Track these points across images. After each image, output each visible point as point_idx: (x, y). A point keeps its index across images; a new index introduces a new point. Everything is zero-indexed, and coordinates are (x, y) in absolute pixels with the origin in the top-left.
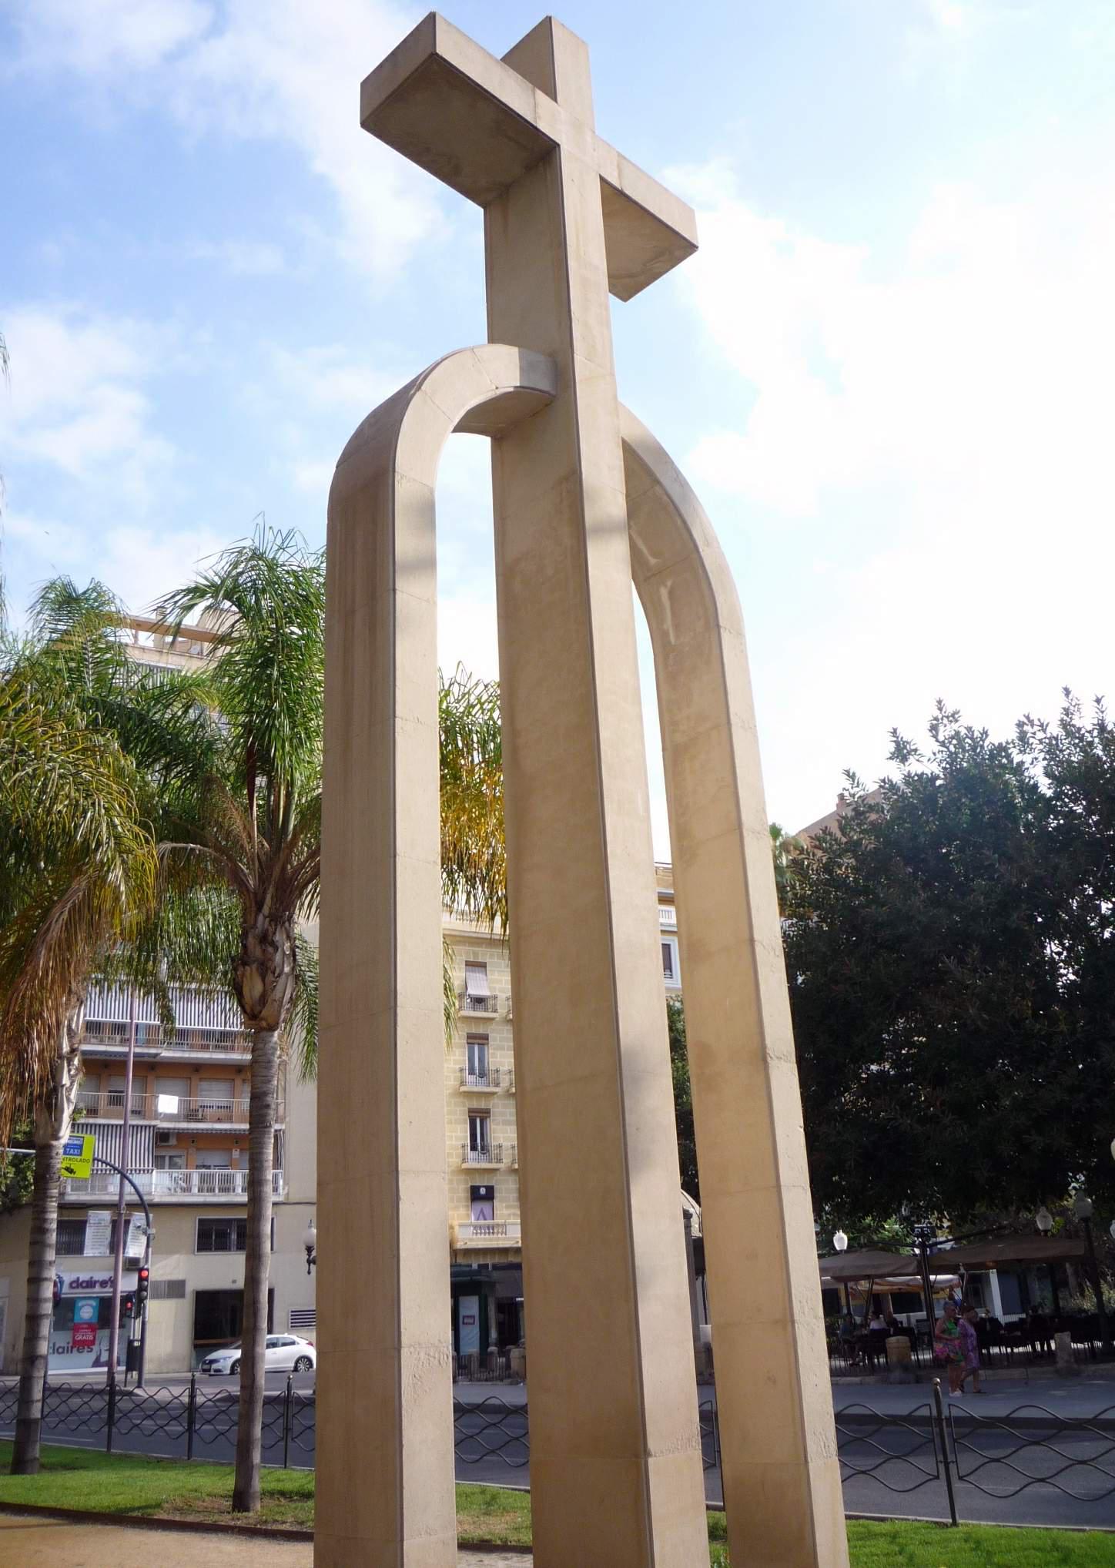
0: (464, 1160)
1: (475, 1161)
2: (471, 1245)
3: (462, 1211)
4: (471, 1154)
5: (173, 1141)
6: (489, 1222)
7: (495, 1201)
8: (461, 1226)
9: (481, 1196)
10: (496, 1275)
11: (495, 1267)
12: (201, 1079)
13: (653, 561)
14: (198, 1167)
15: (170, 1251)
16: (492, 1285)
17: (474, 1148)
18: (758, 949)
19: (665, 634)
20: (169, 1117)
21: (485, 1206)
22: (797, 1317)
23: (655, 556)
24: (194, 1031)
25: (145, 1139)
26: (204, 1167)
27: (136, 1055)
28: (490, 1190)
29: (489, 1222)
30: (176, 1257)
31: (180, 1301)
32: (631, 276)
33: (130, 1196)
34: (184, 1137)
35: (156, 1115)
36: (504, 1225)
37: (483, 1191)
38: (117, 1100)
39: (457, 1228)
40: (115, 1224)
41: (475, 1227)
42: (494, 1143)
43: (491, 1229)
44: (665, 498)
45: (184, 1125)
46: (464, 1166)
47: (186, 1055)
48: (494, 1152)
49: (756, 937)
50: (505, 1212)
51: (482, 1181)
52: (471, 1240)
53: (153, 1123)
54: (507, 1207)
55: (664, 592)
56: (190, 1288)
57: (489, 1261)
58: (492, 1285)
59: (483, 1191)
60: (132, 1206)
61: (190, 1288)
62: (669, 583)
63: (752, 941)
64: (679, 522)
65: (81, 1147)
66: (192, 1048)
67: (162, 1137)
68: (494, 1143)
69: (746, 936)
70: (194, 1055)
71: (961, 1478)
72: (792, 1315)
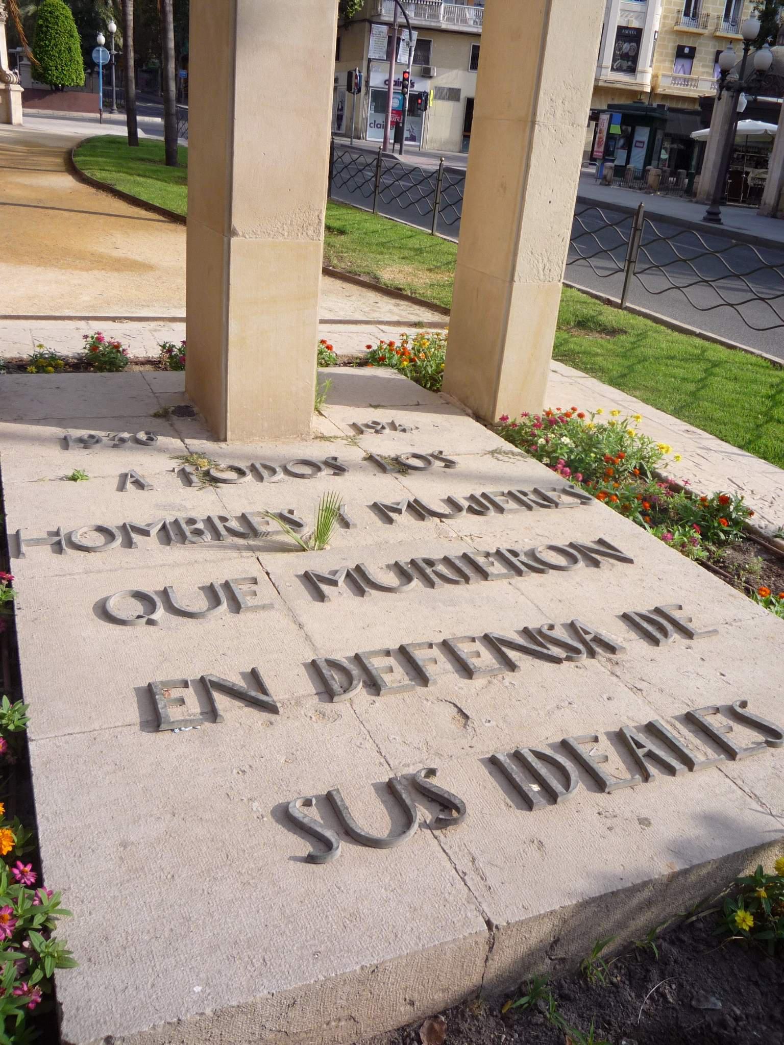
0: (677, 23)
1: (685, 25)
2: (668, 92)
3: (667, 64)
4: (684, 19)
6: (687, 76)
7: (695, 61)
8: (663, 76)
9: (685, 54)
10: (669, 115)
11: (671, 110)
15: (452, 67)
16: (664, 121)
17: (686, 14)
21: (686, 62)
22: (540, 118)
26: (480, 5)
28: (693, 50)
29: (687, 76)
30: (455, 72)
31: (456, 103)
33: (401, 20)
36: (697, 80)
37: (687, 50)
39: (660, 77)
40: (390, 39)
41: (675, 78)
42: (704, 12)
43: (686, 81)
46: (676, 28)
48: (702, 19)
50: (701, 69)
51: (687, 42)
52: (669, 88)
54: (703, 66)
56: (463, 95)
57: (668, 104)
58: (664, 121)
59: (687, 50)
60: (402, 26)
61: (463, 95)
68: (704, 12)
71: (634, 274)
72: (534, 114)
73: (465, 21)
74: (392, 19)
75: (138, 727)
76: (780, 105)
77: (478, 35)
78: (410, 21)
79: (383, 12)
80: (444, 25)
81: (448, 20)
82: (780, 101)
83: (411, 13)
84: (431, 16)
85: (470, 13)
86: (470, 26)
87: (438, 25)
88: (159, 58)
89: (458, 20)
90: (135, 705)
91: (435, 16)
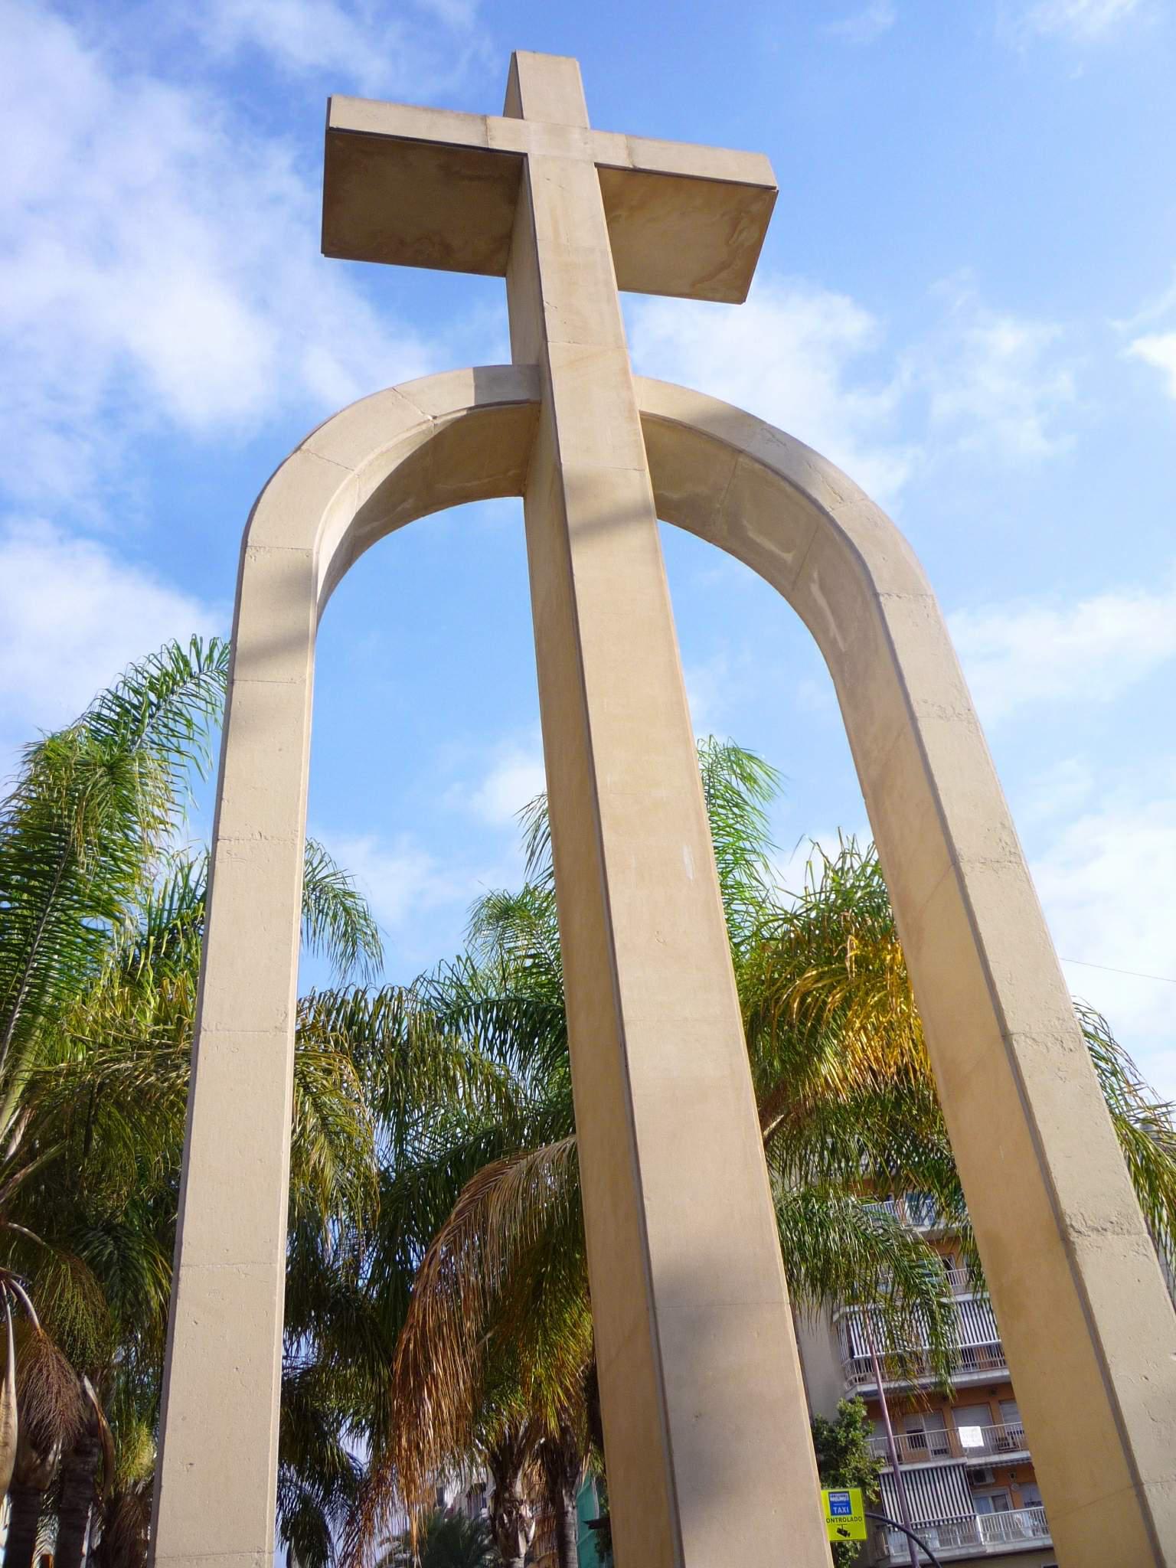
5: (990, 1480)
12: (1000, 1402)
13: (789, 557)
14: (1028, 1505)
18: (1021, 1047)
19: (834, 642)
20: (976, 1452)
23: (788, 551)
24: (979, 1348)
25: (956, 1481)
26: (1033, 1504)
27: (886, 1391)
32: (724, 266)
34: (997, 1470)
35: (962, 1452)
38: (918, 1441)
44: (757, 466)
45: (995, 1458)
47: (975, 1377)
49: (1011, 1026)
53: (961, 1461)
55: (815, 589)
62: (815, 575)
63: (1006, 1036)
64: (789, 489)
65: (848, 1504)
66: (982, 1367)
67: (976, 1477)
69: (996, 1031)
70: (983, 1376)
73: (1018, 1534)
74: (909, 1559)
75: (325, 978)
76: (1008, 1377)
77: (1048, 1550)
78: (935, 1555)
79: (892, 1551)
80: (990, 1548)
81: (993, 1538)
82: (1006, 1373)
83: (934, 1544)
84: (965, 1539)
85: (1022, 1517)
86: (1029, 1539)
87: (980, 1549)
88: (381, 1430)
89: (1007, 1535)
90: (400, 461)
91: (971, 1538)
